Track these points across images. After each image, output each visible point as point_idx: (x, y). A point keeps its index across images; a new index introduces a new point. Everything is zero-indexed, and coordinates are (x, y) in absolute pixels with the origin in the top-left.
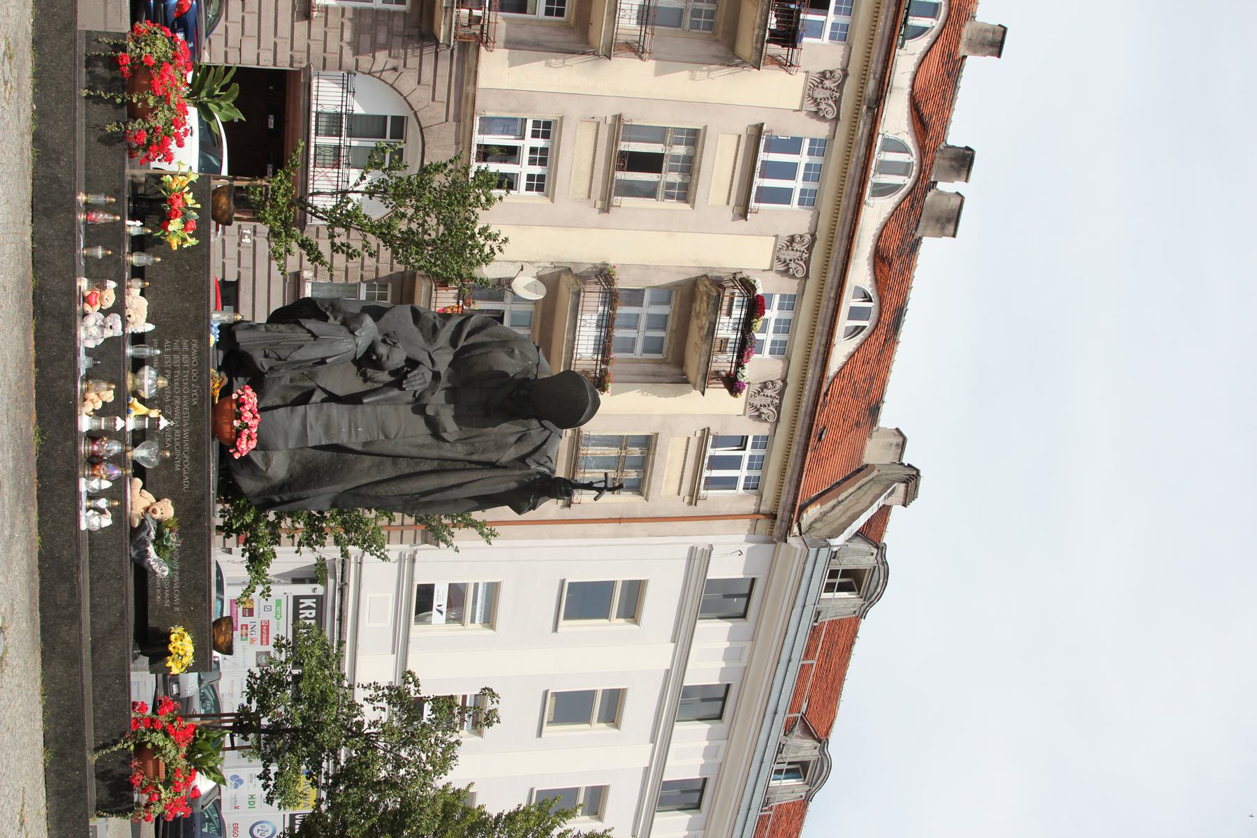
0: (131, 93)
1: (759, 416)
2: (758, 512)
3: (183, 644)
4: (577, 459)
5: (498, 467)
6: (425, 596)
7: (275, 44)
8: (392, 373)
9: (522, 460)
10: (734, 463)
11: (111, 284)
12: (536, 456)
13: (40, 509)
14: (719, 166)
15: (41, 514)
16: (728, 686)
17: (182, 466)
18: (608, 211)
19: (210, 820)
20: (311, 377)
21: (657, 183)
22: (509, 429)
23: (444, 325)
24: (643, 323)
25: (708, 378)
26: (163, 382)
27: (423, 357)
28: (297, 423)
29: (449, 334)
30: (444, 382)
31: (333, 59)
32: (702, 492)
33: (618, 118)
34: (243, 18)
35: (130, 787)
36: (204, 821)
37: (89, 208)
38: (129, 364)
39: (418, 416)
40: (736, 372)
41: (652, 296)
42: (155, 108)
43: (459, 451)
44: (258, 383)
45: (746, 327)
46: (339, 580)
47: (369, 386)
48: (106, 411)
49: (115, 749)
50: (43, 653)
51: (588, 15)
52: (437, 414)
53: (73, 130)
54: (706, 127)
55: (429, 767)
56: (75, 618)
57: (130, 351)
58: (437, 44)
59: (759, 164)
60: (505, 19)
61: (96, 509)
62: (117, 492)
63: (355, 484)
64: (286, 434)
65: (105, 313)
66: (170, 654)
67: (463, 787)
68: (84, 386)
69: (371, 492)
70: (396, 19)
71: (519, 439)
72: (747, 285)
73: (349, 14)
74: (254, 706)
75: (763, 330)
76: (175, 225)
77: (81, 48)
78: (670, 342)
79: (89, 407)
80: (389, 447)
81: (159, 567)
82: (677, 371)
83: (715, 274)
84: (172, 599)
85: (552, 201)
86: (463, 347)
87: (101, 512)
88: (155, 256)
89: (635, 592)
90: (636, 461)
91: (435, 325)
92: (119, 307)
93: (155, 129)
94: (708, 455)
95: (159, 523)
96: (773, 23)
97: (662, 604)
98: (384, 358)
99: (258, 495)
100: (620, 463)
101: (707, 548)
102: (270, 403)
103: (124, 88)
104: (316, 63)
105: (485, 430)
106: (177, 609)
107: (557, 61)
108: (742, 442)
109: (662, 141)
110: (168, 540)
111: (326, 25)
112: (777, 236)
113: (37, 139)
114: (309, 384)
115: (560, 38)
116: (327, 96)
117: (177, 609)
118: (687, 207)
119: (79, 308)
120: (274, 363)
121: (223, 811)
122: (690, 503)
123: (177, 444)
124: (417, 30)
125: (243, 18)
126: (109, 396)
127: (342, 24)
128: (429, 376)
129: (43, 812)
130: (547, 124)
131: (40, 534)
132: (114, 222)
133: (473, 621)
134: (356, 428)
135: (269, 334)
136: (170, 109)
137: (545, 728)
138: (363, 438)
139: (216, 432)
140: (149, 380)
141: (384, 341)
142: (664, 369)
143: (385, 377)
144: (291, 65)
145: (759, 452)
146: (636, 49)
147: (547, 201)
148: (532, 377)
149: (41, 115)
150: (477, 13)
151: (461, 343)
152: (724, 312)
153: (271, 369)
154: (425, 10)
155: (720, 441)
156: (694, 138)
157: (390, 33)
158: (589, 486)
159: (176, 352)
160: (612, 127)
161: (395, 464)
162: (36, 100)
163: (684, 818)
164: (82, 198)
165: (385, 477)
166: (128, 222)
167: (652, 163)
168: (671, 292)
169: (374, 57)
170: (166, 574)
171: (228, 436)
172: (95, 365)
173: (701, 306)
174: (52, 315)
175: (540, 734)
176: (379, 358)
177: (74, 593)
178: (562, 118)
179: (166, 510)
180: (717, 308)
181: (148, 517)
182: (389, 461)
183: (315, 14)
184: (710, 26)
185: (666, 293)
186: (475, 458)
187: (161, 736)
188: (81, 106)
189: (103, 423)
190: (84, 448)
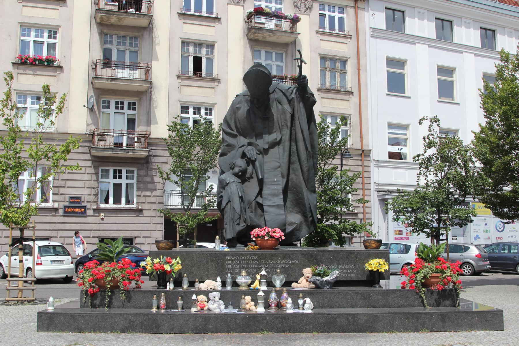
0: (105, 288)
1: (310, 8)
2: (355, 7)
3: (374, 264)
6: (393, 156)
7: (153, 224)
8: (248, 165)
9: (290, 101)
10: (332, 19)
11: (194, 297)
12: (288, 94)
13: (300, 332)
14: (197, 31)
15: (302, 332)
16: (436, 18)
17: (287, 264)
19: (493, 249)
20: (250, 203)
21: (207, 59)
22: (275, 109)
23: (226, 141)
25: (292, 32)
26: (244, 273)
27: (241, 150)
29: (231, 139)
30: (253, 140)
31: (158, 200)
32: (346, 33)
33: (178, 77)
34: (143, 237)
35: (444, 290)
36: (493, 252)
37: (158, 307)
38: (235, 289)
40: (289, 19)
41: (257, 59)
42: (113, 277)
43: (286, 132)
45: (269, 15)
46: (386, 193)
47: (254, 176)
48: (255, 300)
49: (424, 297)
50: (372, 332)
51: (134, 92)
52: (268, 143)
53: (120, 314)
54: (181, 38)
55: (457, 149)
56: (354, 316)
57: (229, 288)
58: (149, 156)
59: (196, 14)
60: (138, 127)
61: (304, 305)
62: (295, 296)
63: (303, 182)
65: (209, 299)
66: (378, 270)
67: (473, 135)
68: (243, 310)
70: (140, 174)
71: (280, 103)
72: (250, 16)
73: (139, 193)
74: (427, 230)
75: (270, 8)
76: (167, 268)
77: (89, 310)
79: (253, 308)
80: (285, 166)
81: (334, 275)
82: (290, 46)
83: (246, 31)
84: (353, 269)
85: (216, 104)
86: (237, 132)
87: (304, 303)
88: (184, 277)
89: (391, 62)
90: (332, 64)
91: (227, 146)
92: (206, 293)
93: (123, 277)
94: (328, 31)
95: (314, 275)
96: (132, 10)
97: (397, 50)
98: (240, 169)
99: (309, 228)
100: (333, 71)
101: (371, 30)
102: (263, 223)
103: (105, 291)
104: (160, 207)
105: (275, 120)
106: (358, 266)
107: (154, 104)
108: (323, 16)
109: (188, 57)
110: (321, 271)
111: (144, 203)
112: (228, 4)
113: (123, 331)
114: (254, 204)
115: (145, 103)
116: (175, 201)
117: (358, 266)
118: (216, 45)
119: (206, 312)
120: (242, 220)
121: (490, 243)
122: (351, 38)
123: (276, 266)
124: (145, 165)
125: (143, 237)
126: (248, 298)
127: (144, 196)
128: (250, 147)
129: (452, 333)
130: (183, 107)
131: (312, 332)
132: (165, 295)
133: (405, 134)
135: (228, 223)
136: (114, 270)
137: (455, 102)
138: (280, 178)
139: (273, 248)
140: (243, 279)
141: (233, 169)
142: (289, 52)
143: (250, 168)
144: (162, 217)
145: (327, 8)
146: (148, 70)
147: (216, 106)
149: (112, 329)
150: (136, 140)
151: (235, 133)
152: (262, 26)
153: (245, 222)
154: (136, 162)
155: (322, 26)
156: (185, 43)
157: (147, 176)
158: (300, 68)
159: (232, 266)
160: (182, 79)
161: (293, 163)
162: (106, 332)
163: (499, 37)
164: (154, 310)
165: (299, 167)
166: (168, 289)
167: (198, 62)
168: (255, 51)
169: (157, 182)
170: (337, 272)
171: (273, 242)
172: (232, 305)
173: (260, 36)
174: (207, 325)
175: (458, 104)
176: (241, 171)
177: (340, 316)
178: (180, 101)
179: (308, 271)
180: (261, 29)
181: (310, 280)
182: (292, 166)
183: (140, 207)
184: (136, 38)
185: (254, 51)
186: (289, 124)
187: (418, 275)
188: (113, 311)
189: (261, 301)
190: (273, 311)
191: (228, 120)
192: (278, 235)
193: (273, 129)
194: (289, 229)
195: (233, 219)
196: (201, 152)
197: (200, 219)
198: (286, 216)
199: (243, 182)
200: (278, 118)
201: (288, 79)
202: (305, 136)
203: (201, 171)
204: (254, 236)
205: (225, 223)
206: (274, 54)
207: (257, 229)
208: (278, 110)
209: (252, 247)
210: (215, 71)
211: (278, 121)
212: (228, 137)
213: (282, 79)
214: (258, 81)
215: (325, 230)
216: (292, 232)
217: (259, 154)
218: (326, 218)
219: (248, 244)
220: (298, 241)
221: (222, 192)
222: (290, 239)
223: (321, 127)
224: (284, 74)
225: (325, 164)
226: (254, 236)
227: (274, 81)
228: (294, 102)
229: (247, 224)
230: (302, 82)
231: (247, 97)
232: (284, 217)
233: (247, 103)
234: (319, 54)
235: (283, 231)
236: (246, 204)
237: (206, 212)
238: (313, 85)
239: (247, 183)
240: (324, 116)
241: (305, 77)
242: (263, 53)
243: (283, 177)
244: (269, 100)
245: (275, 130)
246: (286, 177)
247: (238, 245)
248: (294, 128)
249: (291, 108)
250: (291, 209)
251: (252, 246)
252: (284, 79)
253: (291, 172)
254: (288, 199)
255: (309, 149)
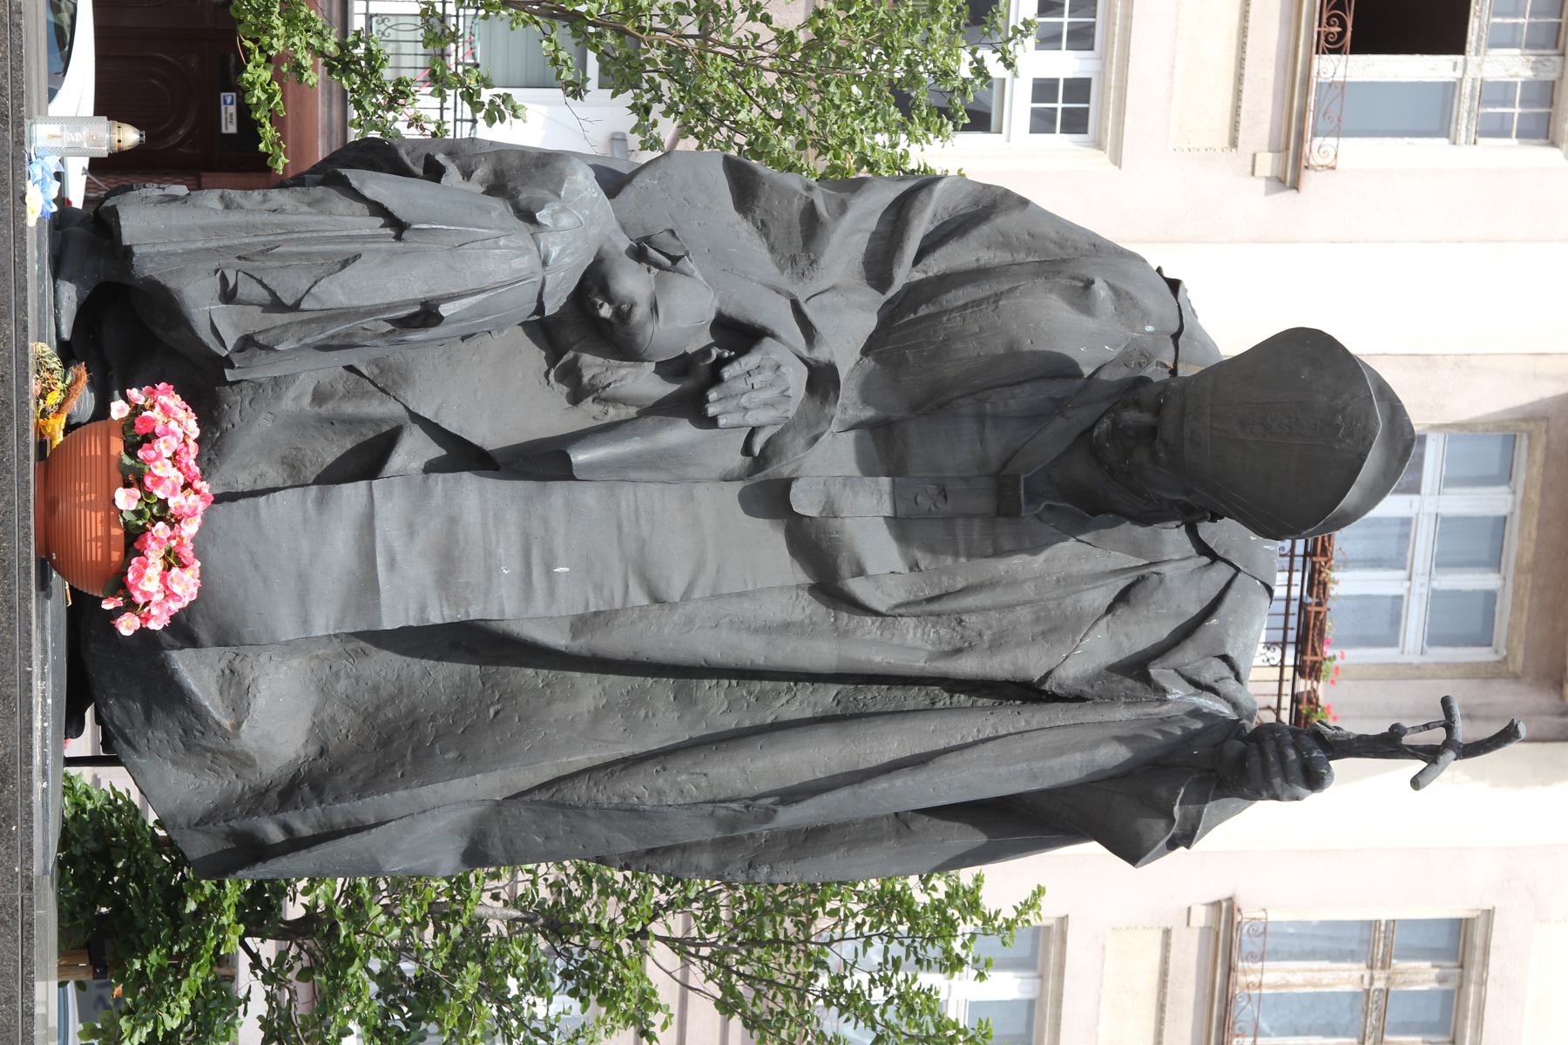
4: (1227, 1002)
5: (1054, 698)
8: (668, 369)
9: (1137, 669)
12: (1187, 656)
18: (1295, 186)
21: (1449, 91)
22: (1081, 562)
23: (843, 208)
24: (1423, 545)
27: (774, 313)
28: (340, 543)
30: (849, 405)
39: (763, 524)
41: (1450, 459)
43: (912, 647)
44: (205, 383)
52: (831, 511)
63: (547, 770)
64: (302, 578)
69: (607, 794)
71: (1123, 597)
78: (1517, 606)
85: (1117, 160)
98: (641, 312)
102: (243, 482)
114: (381, 409)
120: (255, 320)
128: (797, 377)
134: (548, 568)
135: (234, 217)
138: (573, 599)
147: (1098, 161)
148: (1156, 374)
151: (904, 274)
153: (247, 343)
158: (1387, 745)
161: (684, 700)
165: (653, 742)
168: (1510, 442)
171: (94, 552)
176: (623, 315)
182: (664, 688)
186: (968, 666)
191: (1000, 222)
192: (148, 580)
193: (932, 549)
194: (195, 671)
195: (266, 252)
196: (767, 35)
197: (267, 29)
198: (292, 648)
199: (545, 330)
200: (1013, 582)
201: (1303, 685)
202: (882, 784)
203: (621, 33)
204: (137, 410)
205: (235, 194)
206: (1486, 581)
207: (194, 431)
208: (1073, 583)
209: (54, 398)
210: (1354, 152)
211: (992, 584)
212: (872, 224)
213: (1301, 644)
214: (1283, 440)
215: (193, 955)
216: (169, 695)
217: (747, 449)
218: (282, 956)
219: (81, 371)
220: (107, 742)
221: (467, 174)
222: (117, 676)
223: (953, 912)
224: (1340, 655)
225: (679, 945)
226: (137, 410)
227: (1275, 563)
228: (1133, 702)
229: (228, 362)
230: (1282, 758)
231: (1168, 357)
232: (288, 629)
233: (1123, 360)
234: (1489, 914)
235: (183, 629)
236: (382, 350)
237: (314, 77)
238: (1254, 850)
239: (536, 357)
240: (1037, 946)
241: (1314, 780)
242: (1493, 501)
243: (581, 624)
244: (1145, 519)
245: (925, 561)
246: (580, 645)
247: (69, 294)
248: (944, 699)
249: (1091, 680)
250: (342, 686)
251: (68, 392)
252: (1300, 652)
253: (619, 684)
254: (417, 666)
255: (790, 817)
